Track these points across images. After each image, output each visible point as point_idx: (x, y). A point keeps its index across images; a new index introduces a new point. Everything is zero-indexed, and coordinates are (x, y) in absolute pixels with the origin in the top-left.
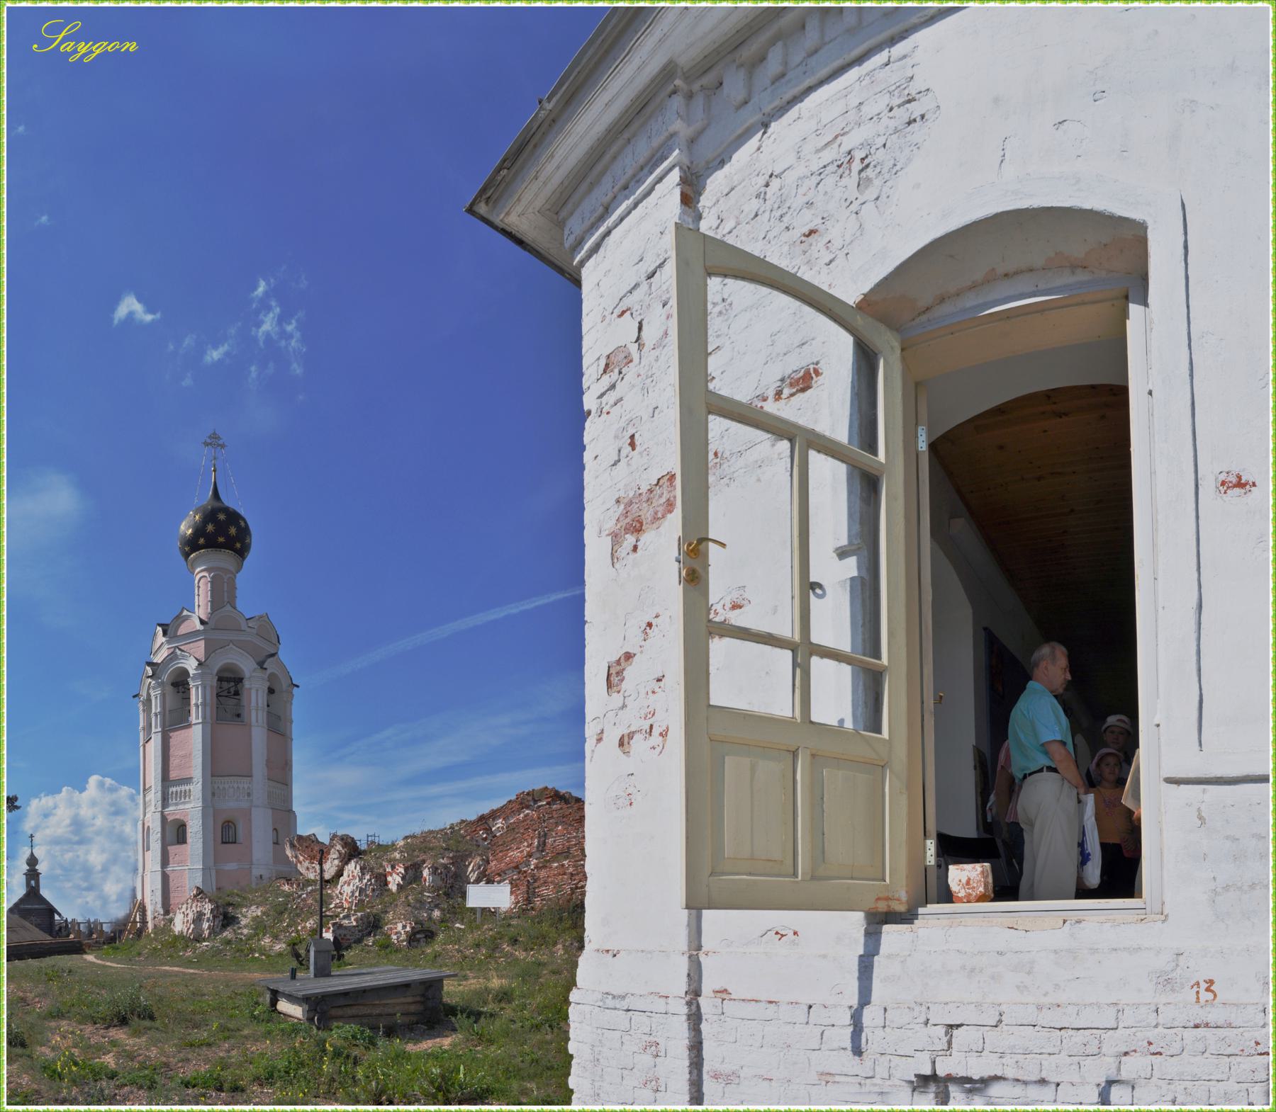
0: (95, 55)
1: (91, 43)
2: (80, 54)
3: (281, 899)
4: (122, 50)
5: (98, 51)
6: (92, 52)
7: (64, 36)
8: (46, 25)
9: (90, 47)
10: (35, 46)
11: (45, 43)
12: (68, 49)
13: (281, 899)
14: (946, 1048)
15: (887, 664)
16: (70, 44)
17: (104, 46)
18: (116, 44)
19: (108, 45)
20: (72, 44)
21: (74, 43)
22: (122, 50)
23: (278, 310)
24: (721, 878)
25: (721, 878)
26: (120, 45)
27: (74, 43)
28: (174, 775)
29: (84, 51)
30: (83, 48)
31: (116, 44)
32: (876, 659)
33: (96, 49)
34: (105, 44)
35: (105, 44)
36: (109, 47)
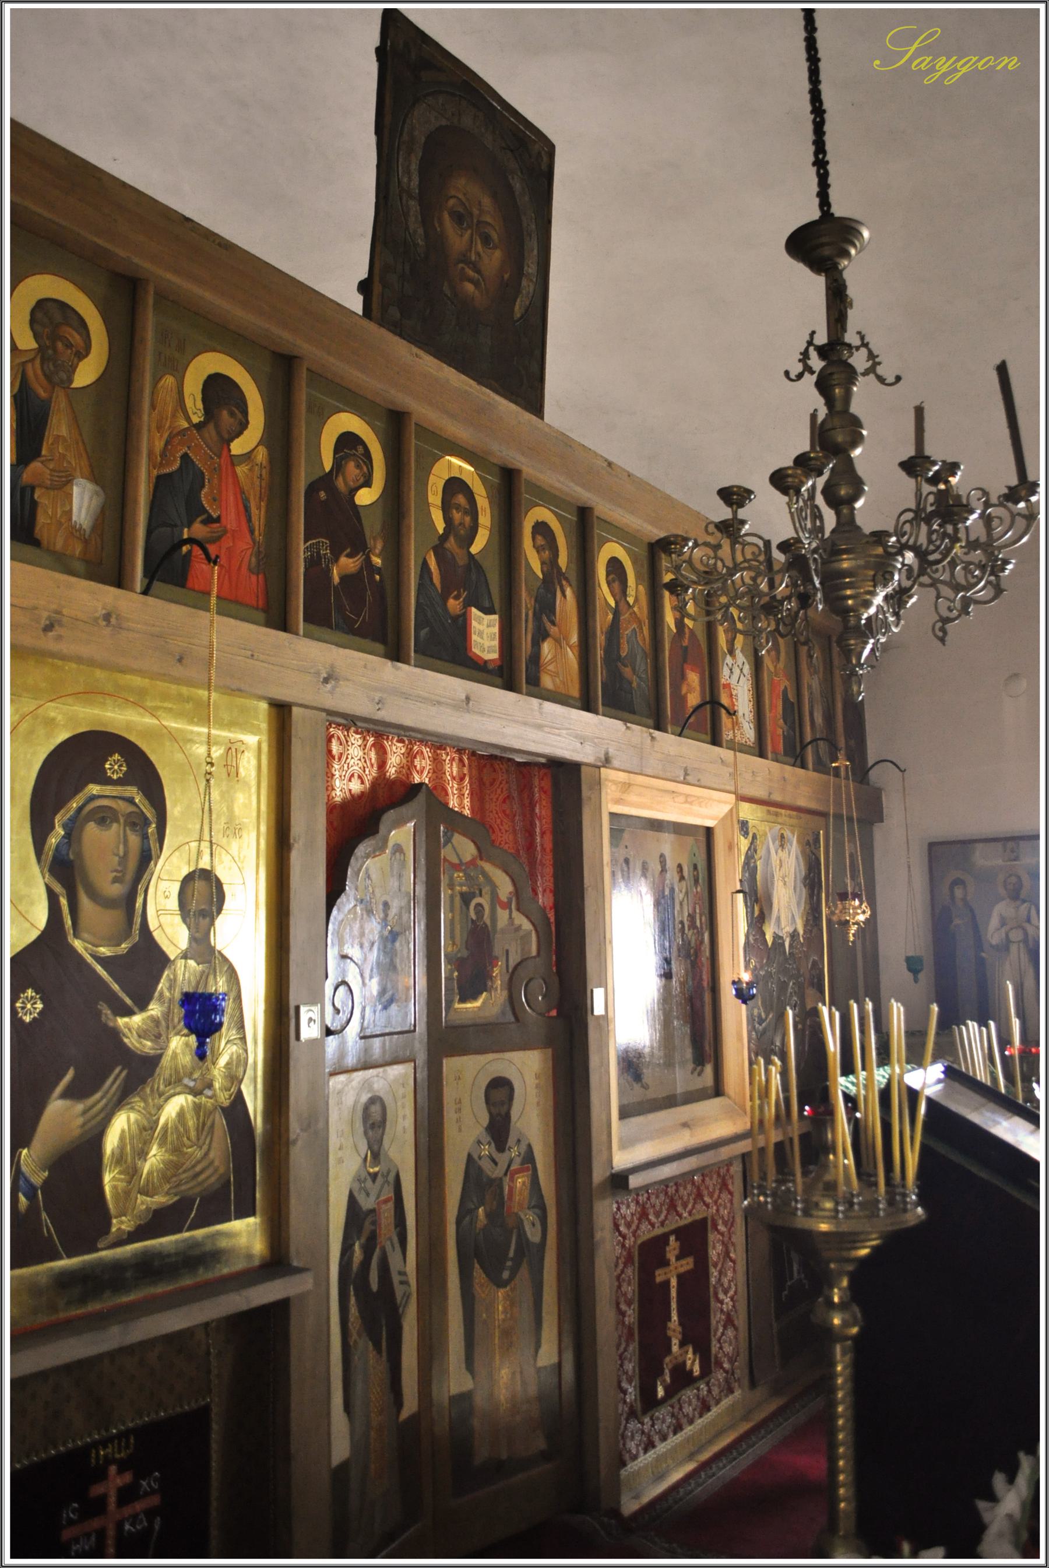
0: (960, 74)
1: (954, 58)
2: (940, 73)
3: (197, 1008)
4: (999, 68)
5: (964, 70)
6: (956, 70)
7: (917, 49)
8: (890, 35)
9: (951, 65)
10: (877, 62)
11: (889, 58)
12: (923, 65)
13: (197, 1008)
14: (91, 829)
15: (74, 385)
16: (925, 59)
17: (972, 62)
18: (989, 60)
19: (978, 61)
20: (928, 59)
21: (931, 58)
22: (999, 68)
23: (803, 489)
24: (384, 1328)
25: (384, 1328)
26: (995, 61)
27: (931, 58)
28: (350, 1061)
29: (944, 69)
30: (943, 65)
31: (989, 60)
32: (707, 1223)
33: (961, 67)
34: (975, 59)
35: (975, 59)
36: (1006, 61)
